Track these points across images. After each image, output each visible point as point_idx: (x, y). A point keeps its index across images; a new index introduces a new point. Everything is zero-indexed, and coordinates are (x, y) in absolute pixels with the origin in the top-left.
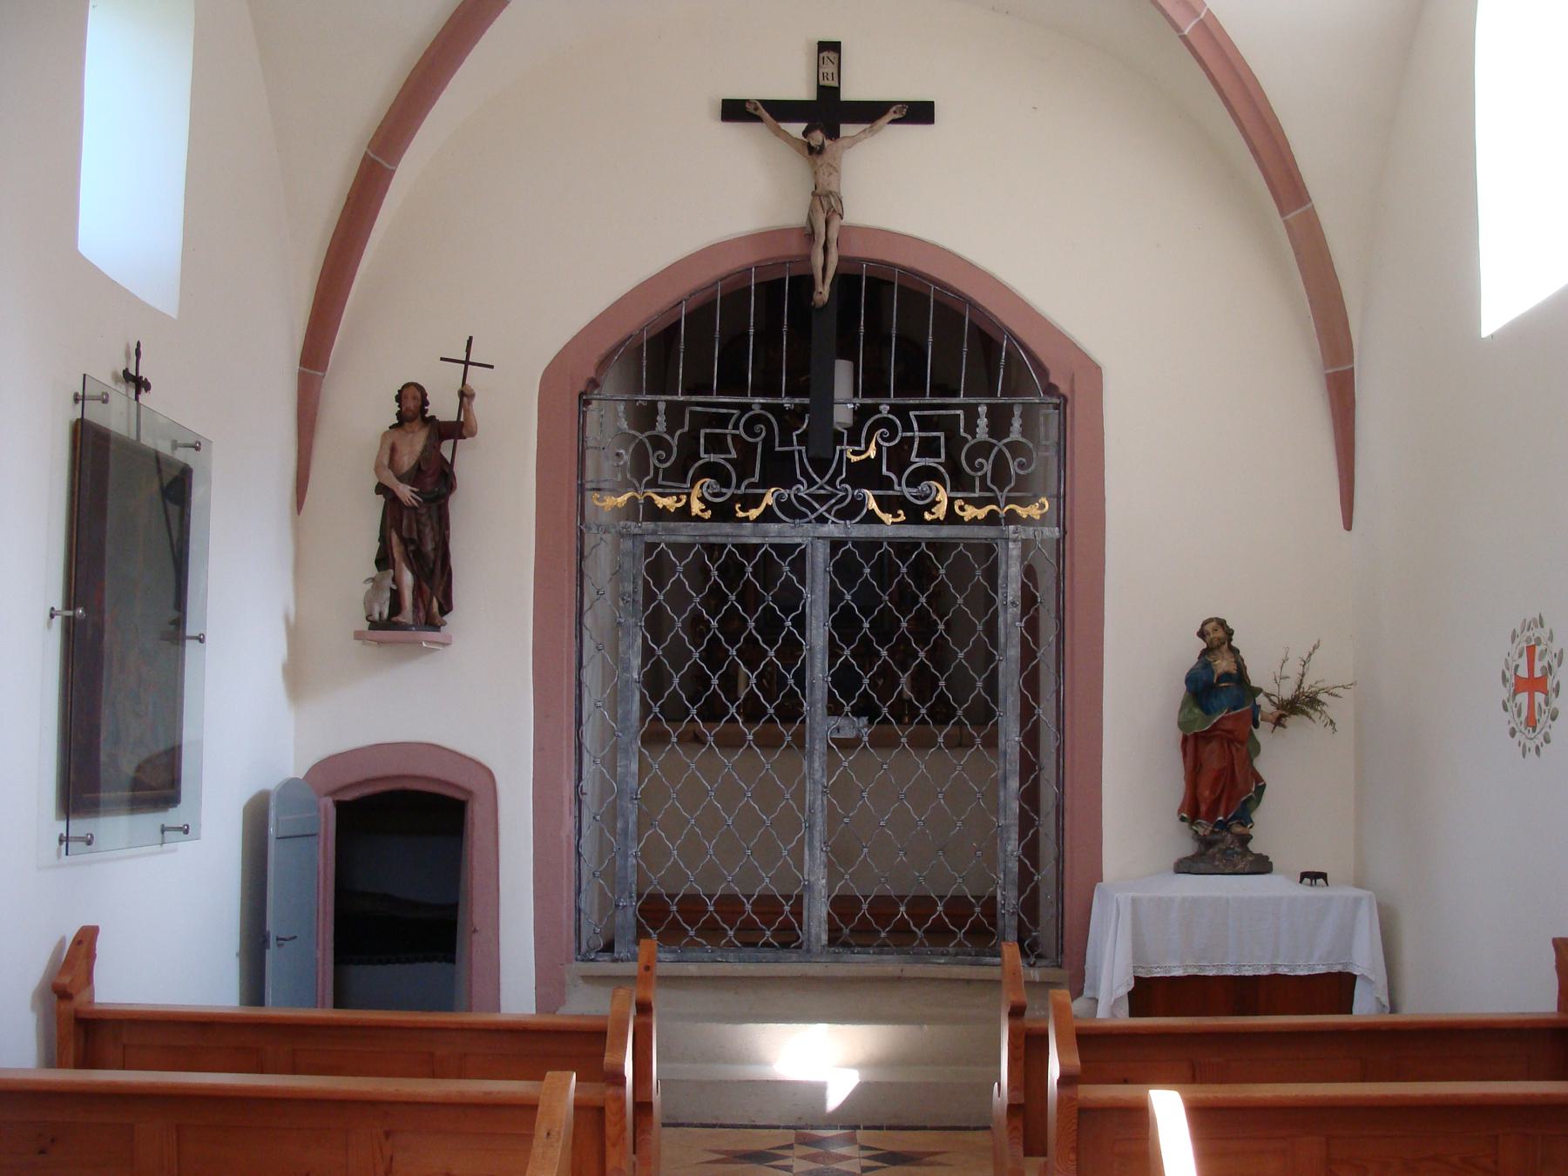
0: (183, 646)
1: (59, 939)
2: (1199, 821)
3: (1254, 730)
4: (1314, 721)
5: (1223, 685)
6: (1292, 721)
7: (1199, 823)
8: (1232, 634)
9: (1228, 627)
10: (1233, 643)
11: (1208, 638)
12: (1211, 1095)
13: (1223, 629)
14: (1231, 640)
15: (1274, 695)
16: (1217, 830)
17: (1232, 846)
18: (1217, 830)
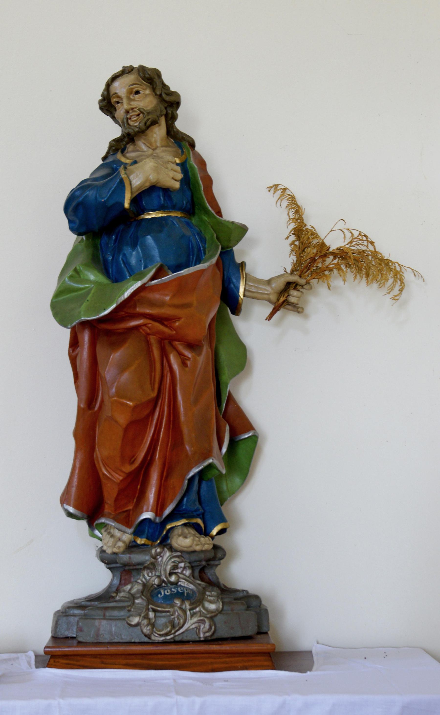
0: (76, 235)
1: (329, 245)
2: (103, 520)
3: (232, 317)
4: (290, 256)
5: (153, 215)
6: (300, 285)
7: (104, 525)
8: (178, 104)
9: (164, 86)
10: (179, 125)
11: (120, 113)
12: (211, 646)
13: (154, 90)
14: (174, 118)
15: (401, 291)
16: (140, 541)
17: (173, 579)
18: (140, 541)
